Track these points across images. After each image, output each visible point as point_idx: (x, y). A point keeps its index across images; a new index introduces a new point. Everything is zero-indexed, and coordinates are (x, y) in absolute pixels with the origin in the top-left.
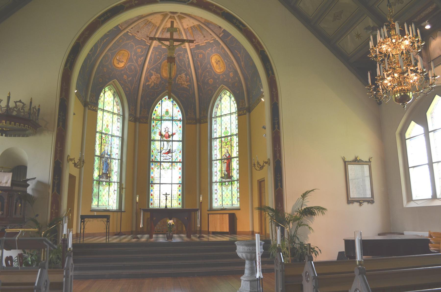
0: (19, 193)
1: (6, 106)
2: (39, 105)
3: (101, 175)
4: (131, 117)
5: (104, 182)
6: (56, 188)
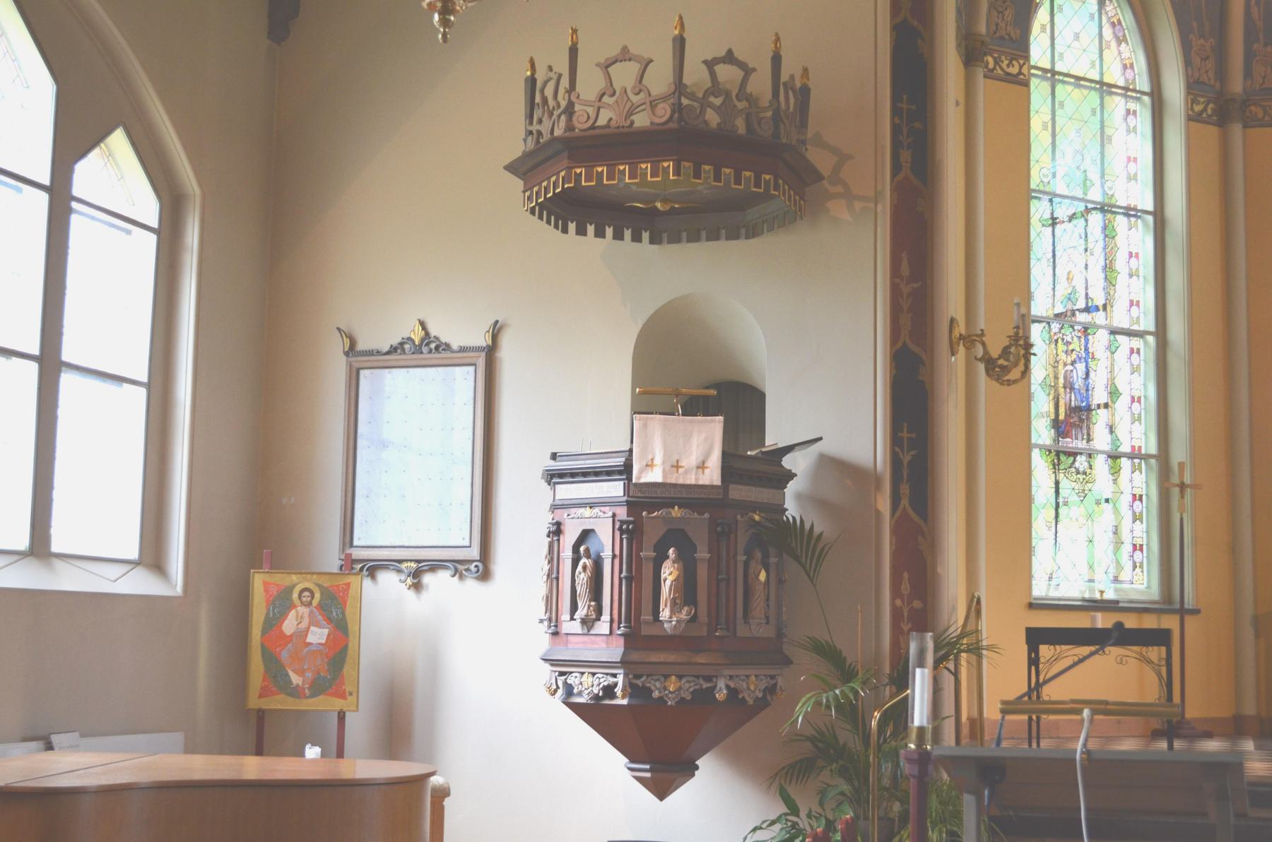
0: (757, 518)
1: (673, 87)
2: (806, 70)
3: (1062, 422)
4: (1202, 100)
5: (1078, 458)
6: (905, 489)
